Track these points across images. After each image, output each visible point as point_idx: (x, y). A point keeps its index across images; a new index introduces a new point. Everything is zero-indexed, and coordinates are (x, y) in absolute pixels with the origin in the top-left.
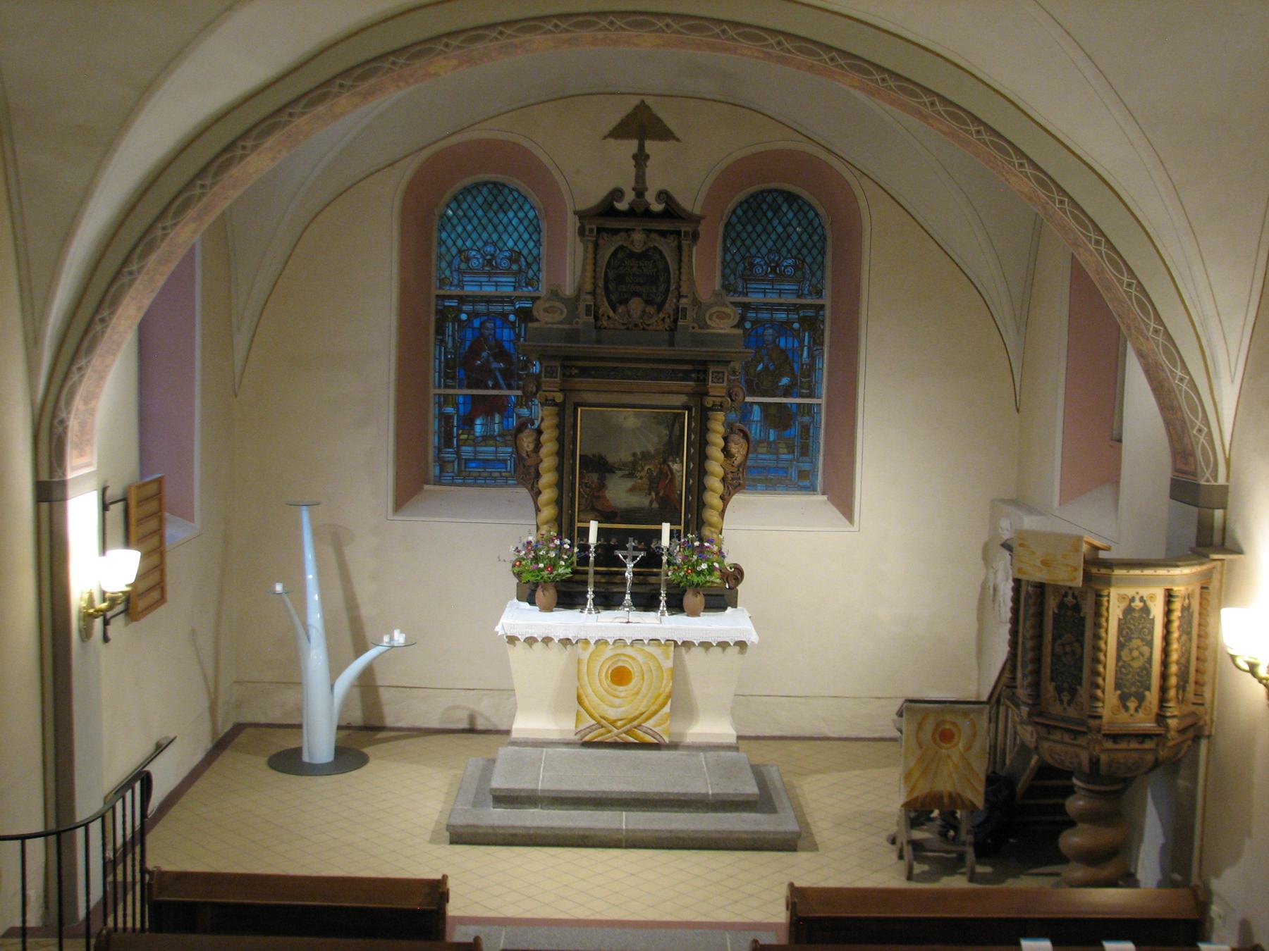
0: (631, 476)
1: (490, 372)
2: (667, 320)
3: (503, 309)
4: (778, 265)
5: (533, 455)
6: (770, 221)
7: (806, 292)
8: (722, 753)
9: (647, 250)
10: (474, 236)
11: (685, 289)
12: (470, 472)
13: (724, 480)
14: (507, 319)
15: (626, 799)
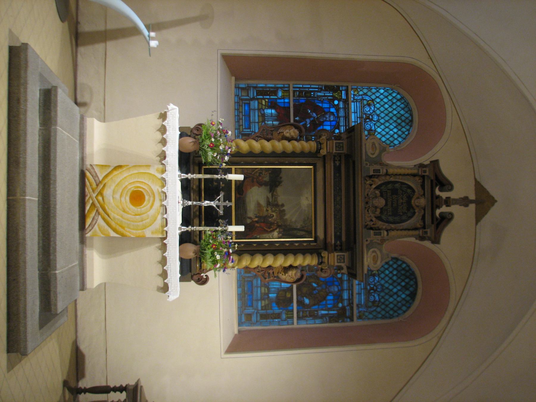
0: (268, 203)
1: (303, 119)
2: (372, 223)
4: (375, 291)
6: (399, 284)
7: (360, 309)
8: (78, 279)
11: (392, 233)
12: (242, 106)
13: (270, 267)
15: (49, 201)
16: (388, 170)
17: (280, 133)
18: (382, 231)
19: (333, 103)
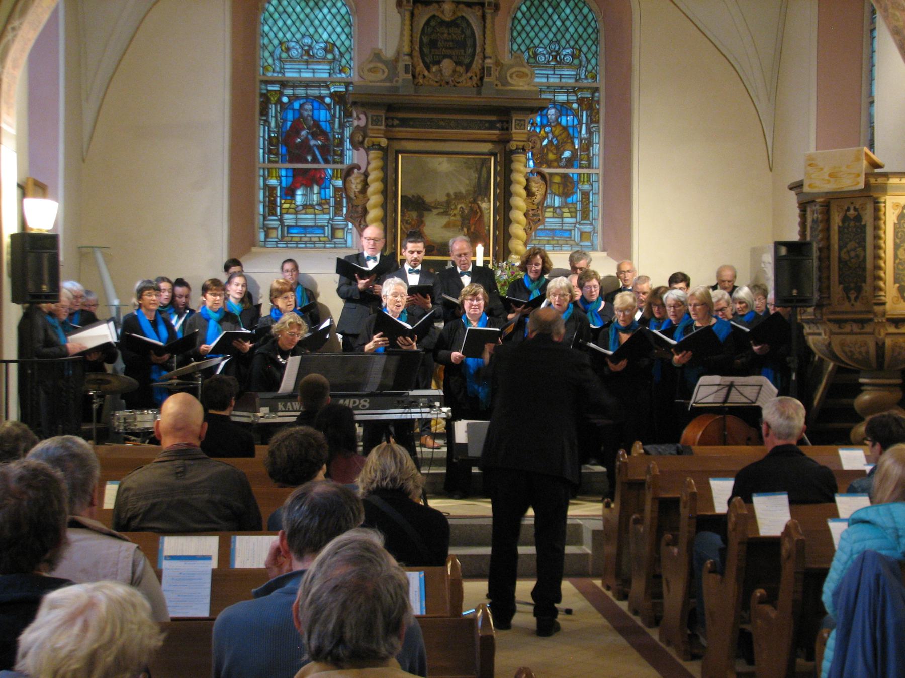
0: (446, 213)
1: (310, 150)
2: (474, 78)
3: (320, 93)
4: (558, 53)
5: (361, 196)
6: (550, 16)
7: (583, 76)
9: (456, 19)
10: (293, 29)
14: (324, 102)
16: (406, 53)
17: (355, 196)
18: (485, 66)
19: (286, 104)
